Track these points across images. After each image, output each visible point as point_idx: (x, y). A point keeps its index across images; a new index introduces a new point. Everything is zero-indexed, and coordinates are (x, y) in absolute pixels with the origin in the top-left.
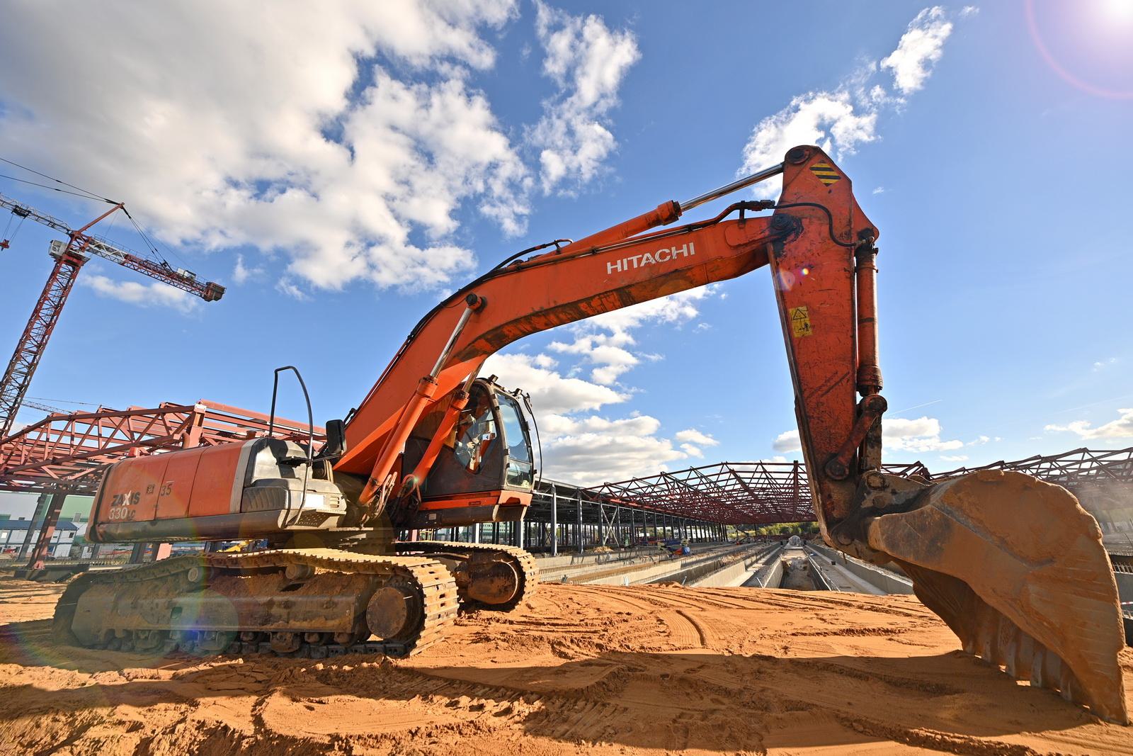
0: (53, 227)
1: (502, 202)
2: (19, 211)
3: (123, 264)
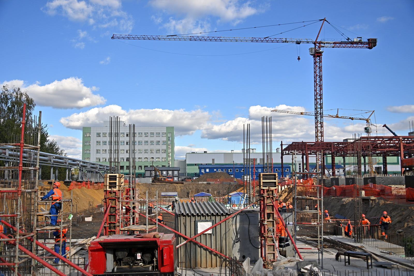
0: (308, 43)
1: (61, 177)
2: (298, 43)
3: (333, 47)
